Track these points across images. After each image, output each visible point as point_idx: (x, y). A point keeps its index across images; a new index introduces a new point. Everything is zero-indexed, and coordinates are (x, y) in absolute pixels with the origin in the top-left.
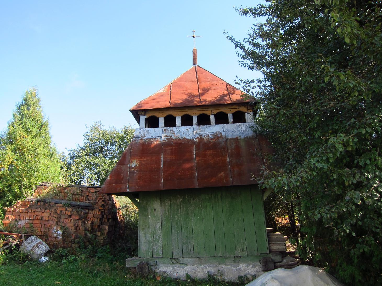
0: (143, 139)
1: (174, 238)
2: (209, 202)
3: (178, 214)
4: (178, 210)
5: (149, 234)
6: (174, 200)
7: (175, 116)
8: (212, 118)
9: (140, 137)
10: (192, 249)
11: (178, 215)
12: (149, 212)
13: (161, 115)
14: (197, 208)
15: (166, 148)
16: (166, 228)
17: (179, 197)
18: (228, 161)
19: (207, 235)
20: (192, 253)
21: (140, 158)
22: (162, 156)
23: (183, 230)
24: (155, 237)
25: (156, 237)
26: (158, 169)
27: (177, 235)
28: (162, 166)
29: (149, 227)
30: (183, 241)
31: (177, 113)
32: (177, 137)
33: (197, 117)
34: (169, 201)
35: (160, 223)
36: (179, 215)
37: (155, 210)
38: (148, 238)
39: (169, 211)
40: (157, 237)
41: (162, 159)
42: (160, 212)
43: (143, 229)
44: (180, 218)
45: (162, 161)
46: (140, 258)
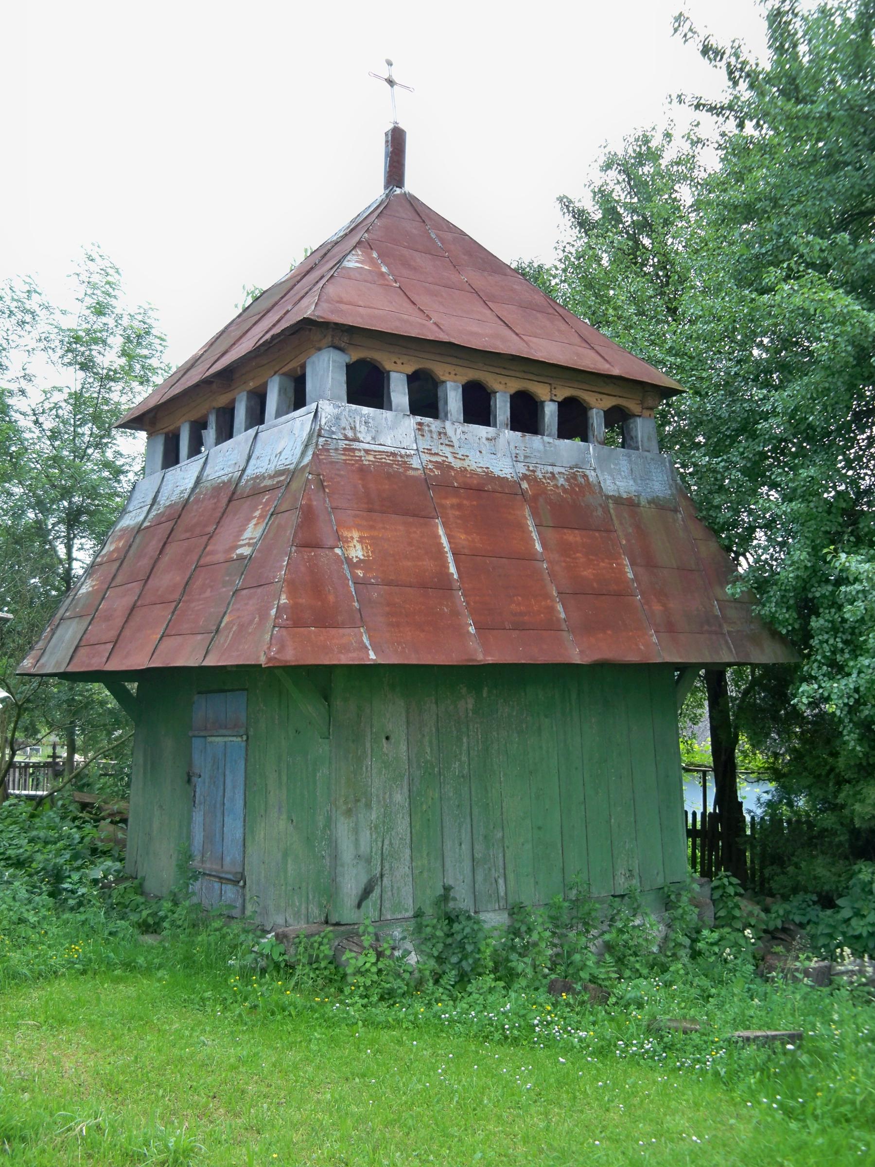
0: (354, 450)
1: (448, 844)
2: (546, 716)
3: (461, 754)
4: (459, 739)
5: (368, 833)
6: (449, 702)
7: (443, 378)
8: (550, 411)
9: (341, 437)
10: (501, 881)
11: (460, 760)
12: (368, 745)
13: (399, 362)
14: (515, 735)
15: (443, 502)
16: (424, 807)
17: (464, 691)
18: (630, 575)
19: (539, 828)
20: (502, 894)
21: (372, 527)
22: (441, 531)
23: (476, 811)
24: (387, 842)
25: (391, 844)
26: (443, 584)
27: (459, 831)
28: (452, 569)
29: (368, 806)
30: (476, 855)
31: (449, 368)
32: (465, 464)
33: (460, 390)
34: (434, 706)
35: (406, 790)
36: (464, 758)
37: (387, 738)
38: (364, 848)
39: (435, 741)
40: (396, 842)
41: (444, 541)
42: (405, 748)
43: (349, 812)
44: (465, 772)
45: (447, 549)
46: (338, 924)
